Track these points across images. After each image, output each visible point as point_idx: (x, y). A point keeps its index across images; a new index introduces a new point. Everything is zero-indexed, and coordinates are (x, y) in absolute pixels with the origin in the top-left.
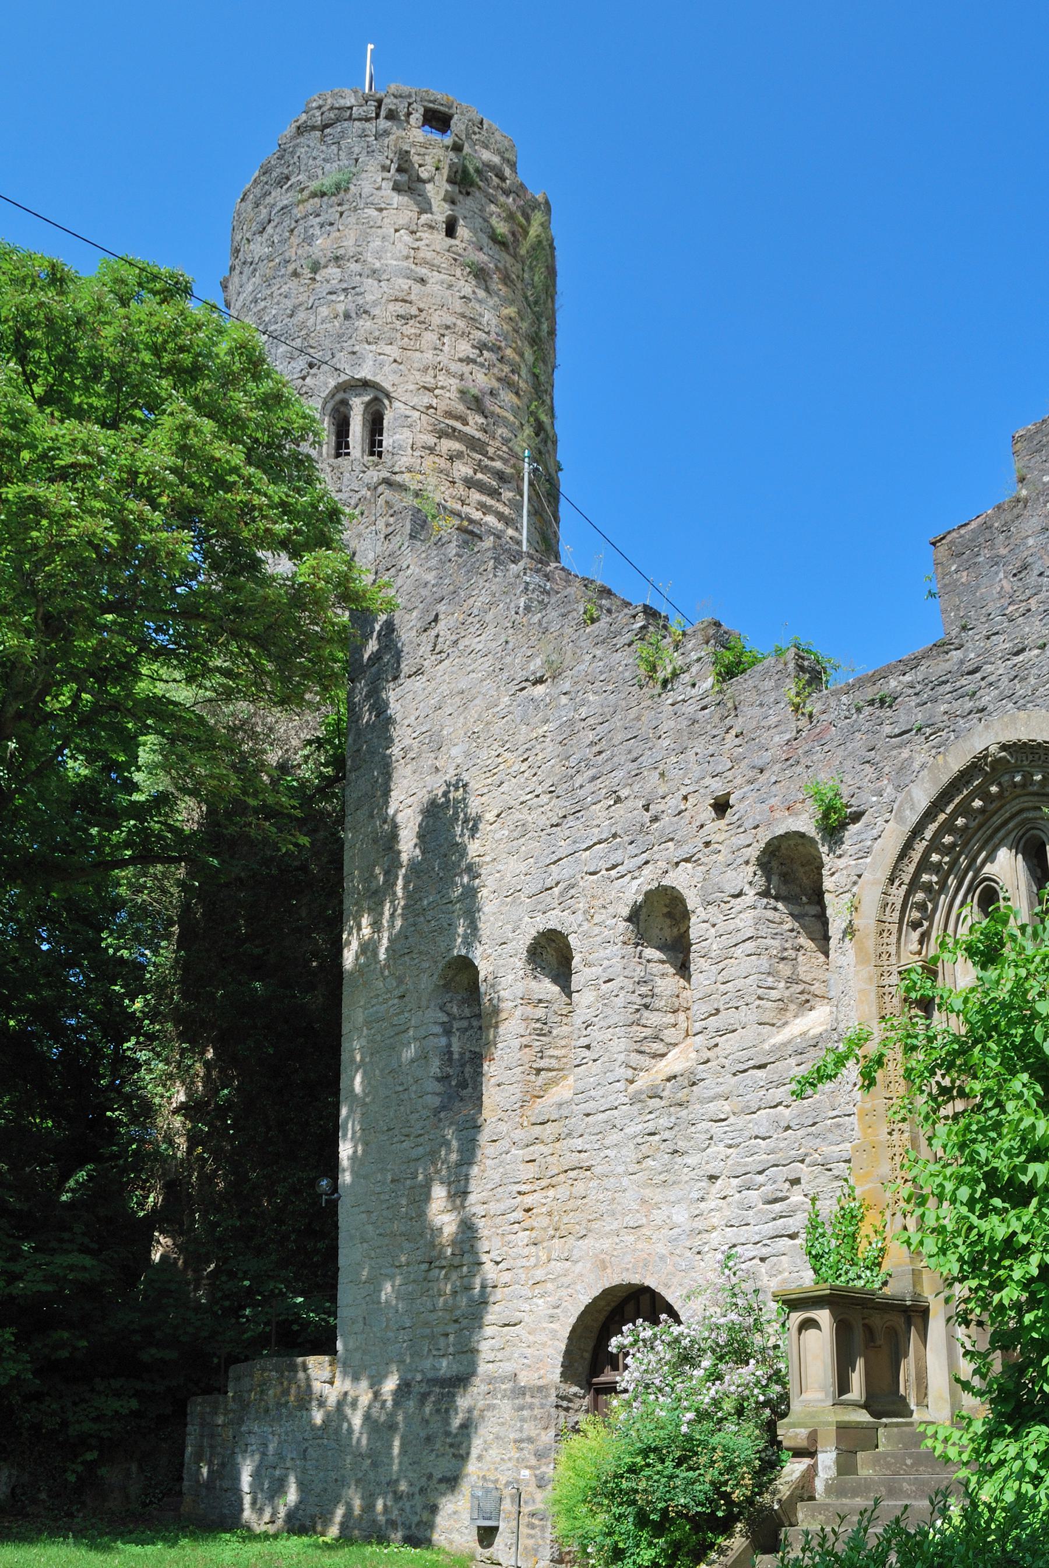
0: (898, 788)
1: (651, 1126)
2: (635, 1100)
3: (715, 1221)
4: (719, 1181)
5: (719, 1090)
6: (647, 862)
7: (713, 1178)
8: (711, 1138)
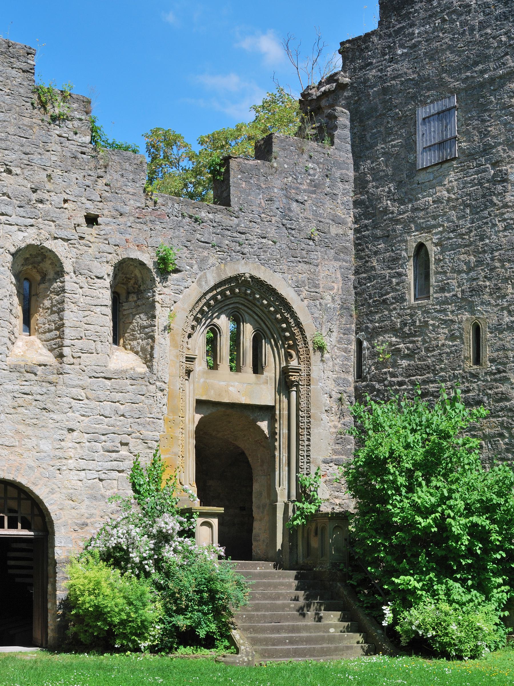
0: (200, 269)
1: (27, 389)
2: (15, 369)
3: (71, 454)
4: (75, 433)
5: (80, 383)
6: (32, 226)
7: (71, 430)
8: (70, 408)
